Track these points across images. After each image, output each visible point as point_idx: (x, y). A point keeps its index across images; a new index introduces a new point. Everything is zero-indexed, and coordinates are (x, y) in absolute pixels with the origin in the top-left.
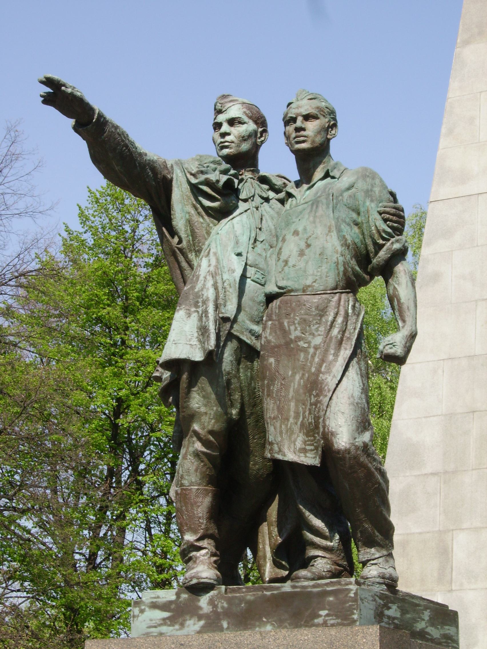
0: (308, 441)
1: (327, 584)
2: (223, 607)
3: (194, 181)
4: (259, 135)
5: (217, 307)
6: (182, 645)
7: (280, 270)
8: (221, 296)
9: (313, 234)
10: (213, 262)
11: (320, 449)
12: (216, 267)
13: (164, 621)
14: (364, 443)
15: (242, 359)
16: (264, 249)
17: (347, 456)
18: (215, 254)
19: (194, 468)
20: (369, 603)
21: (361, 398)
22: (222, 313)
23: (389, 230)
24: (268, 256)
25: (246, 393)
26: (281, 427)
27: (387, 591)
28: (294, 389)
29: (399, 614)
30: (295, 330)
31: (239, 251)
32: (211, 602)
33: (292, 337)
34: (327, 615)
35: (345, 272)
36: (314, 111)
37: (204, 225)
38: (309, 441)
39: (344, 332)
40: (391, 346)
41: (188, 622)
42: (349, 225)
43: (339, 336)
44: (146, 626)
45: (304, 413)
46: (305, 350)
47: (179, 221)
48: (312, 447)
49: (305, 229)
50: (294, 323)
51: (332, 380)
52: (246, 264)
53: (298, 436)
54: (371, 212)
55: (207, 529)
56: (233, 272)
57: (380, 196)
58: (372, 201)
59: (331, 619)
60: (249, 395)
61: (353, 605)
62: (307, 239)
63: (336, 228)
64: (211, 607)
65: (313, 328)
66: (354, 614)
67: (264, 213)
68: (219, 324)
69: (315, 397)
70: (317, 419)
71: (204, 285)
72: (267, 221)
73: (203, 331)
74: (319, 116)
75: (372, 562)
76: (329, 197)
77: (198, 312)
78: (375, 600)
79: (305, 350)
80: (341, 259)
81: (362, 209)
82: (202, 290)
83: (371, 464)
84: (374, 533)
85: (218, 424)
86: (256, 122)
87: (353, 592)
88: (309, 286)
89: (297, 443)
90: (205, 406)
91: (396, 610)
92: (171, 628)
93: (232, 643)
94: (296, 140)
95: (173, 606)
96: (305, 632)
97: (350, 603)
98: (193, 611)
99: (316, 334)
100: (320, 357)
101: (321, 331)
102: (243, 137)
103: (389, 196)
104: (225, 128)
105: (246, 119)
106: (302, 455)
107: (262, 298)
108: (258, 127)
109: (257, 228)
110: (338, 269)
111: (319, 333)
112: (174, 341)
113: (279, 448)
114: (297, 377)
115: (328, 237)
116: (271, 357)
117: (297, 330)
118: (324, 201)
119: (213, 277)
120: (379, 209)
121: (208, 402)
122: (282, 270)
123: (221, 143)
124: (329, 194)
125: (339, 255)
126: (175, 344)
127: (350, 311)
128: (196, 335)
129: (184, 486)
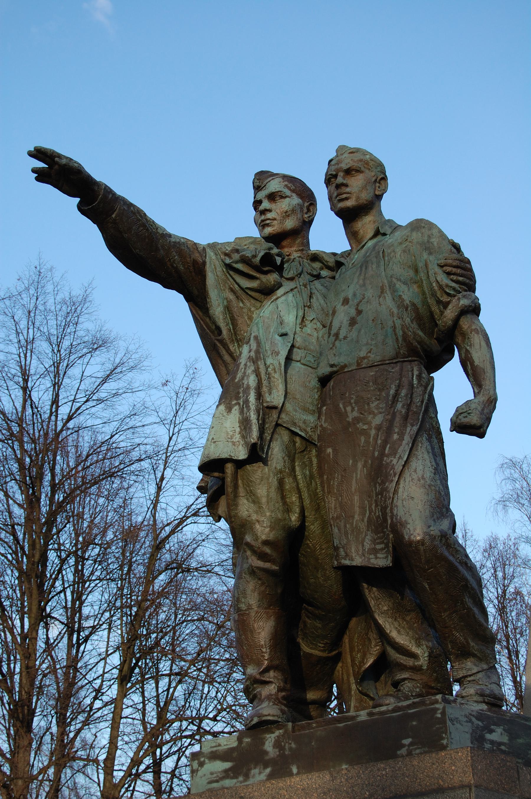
0: (377, 539)
1: (409, 707)
2: (291, 749)
3: (228, 261)
4: (305, 210)
5: (259, 396)
7: (331, 346)
8: (265, 383)
9: (363, 299)
10: (254, 346)
11: (390, 545)
12: (257, 352)
13: (227, 774)
14: (441, 531)
15: (297, 456)
16: (315, 329)
17: (422, 548)
18: (256, 338)
20: (462, 725)
21: (434, 479)
22: (267, 402)
23: (453, 284)
24: (320, 335)
26: (345, 526)
27: (489, 711)
28: (356, 480)
29: (507, 738)
31: (283, 331)
32: (277, 744)
33: (350, 419)
34: (411, 744)
35: (405, 337)
36: (356, 165)
39: (409, 405)
40: (466, 414)
41: (253, 772)
42: (405, 283)
43: (403, 411)
44: (207, 781)
45: (370, 507)
47: (217, 310)
48: (382, 546)
49: (355, 295)
50: (351, 404)
52: (293, 346)
53: (366, 535)
54: (430, 266)
55: (270, 659)
56: (278, 355)
58: (430, 253)
59: (416, 749)
60: (310, 496)
62: (358, 305)
63: (390, 288)
64: (277, 750)
65: (373, 405)
66: (443, 739)
68: (263, 414)
69: (380, 485)
70: (384, 509)
71: (245, 373)
72: (318, 299)
73: (245, 423)
74: (363, 169)
75: (469, 679)
76: (379, 254)
78: (470, 721)
79: (365, 433)
80: (398, 323)
81: (421, 265)
82: (243, 379)
83: (453, 556)
85: (273, 532)
87: (439, 711)
88: (364, 358)
89: (365, 544)
90: (256, 512)
91: (501, 734)
92: (235, 781)
93: (298, 789)
94: (338, 198)
95: (235, 754)
96: (382, 766)
97: (438, 726)
99: (376, 411)
100: (383, 438)
101: (382, 408)
102: (286, 212)
103: (450, 247)
104: (266, 204)
105: (288, 192)
106: (372, 556)
107: (314, 383)
108: (304, 202)
109: (305, 306)
110: (396, 334)
111: (380, 410)
112: (213, 439)
113: (346, 553)
114: (360, 465)
115: (381, 299)
116: (329, 447)
118: (374, 260)
119: (254, 362)
120: (439, 262)
123: (263, 221)
124: (379, 252)
127: (415, 382)
128: (238, 430)
129: (241, 610)
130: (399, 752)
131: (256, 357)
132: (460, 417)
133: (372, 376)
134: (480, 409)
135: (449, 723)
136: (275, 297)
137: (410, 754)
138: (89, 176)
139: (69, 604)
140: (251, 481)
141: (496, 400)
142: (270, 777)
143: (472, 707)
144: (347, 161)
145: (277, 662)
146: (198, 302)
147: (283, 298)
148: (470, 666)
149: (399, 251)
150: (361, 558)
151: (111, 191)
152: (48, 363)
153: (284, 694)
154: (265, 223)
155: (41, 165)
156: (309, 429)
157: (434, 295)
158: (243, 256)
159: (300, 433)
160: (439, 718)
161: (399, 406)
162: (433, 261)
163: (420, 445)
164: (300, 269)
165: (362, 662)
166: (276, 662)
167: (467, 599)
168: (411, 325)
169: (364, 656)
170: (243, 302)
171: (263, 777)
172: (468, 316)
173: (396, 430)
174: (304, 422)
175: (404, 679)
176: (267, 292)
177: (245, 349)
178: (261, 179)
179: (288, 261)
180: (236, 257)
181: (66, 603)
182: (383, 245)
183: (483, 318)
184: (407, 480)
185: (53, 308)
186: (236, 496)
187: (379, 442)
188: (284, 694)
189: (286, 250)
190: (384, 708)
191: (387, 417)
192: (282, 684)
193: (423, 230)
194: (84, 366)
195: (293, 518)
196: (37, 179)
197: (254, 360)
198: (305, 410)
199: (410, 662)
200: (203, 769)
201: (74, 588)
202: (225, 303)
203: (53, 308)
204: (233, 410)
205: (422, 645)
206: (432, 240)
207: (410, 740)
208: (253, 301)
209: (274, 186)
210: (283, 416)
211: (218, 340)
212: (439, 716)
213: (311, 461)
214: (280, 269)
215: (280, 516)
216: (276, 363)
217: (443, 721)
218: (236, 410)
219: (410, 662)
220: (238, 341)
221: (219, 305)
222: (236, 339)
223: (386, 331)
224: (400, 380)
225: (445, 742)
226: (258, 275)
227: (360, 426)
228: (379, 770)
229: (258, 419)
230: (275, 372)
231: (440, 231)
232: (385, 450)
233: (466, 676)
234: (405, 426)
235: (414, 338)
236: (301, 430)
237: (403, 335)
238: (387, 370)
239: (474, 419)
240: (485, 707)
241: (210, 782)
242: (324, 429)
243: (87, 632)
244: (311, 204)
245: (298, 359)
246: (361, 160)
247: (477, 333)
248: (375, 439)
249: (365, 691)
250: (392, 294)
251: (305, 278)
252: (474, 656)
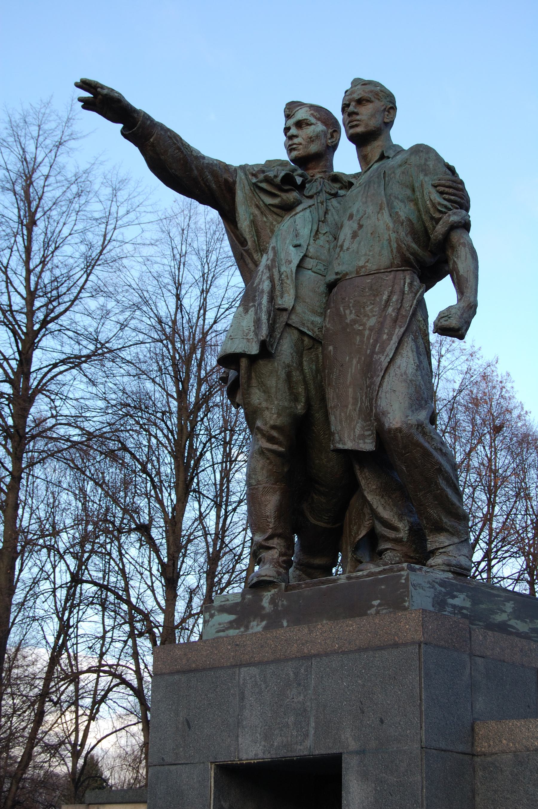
1: (380, 573)
4: (329, 136)
5: (272, 299)
6: (237, 645)
8: (278, 288)
9: (365, 214)
10: (271, 254)
12: (273, 260)
13: (232, 625)
15: (305, 352)
17: (399, 435)
18: (274, 248)
19: (260, 466)
20: (425, 590)
22: (280, 305)
23: (446, 203)
24: (332, 247)
25: (312, 387)
28: (351, 374)
31: (298, 243)
32: (272, 601)
34: (379, 605)
35: (399, 248)
37: (268, 224)
39: (399, 309)
40: (447, 318)
41: (252, 624)
42: (402, 201)
43: (394, 314)
46: (360, 333)
48: (370, 432)
49: (358, 211)
50: (349, 307)
52: (305, 256)
53: (357, 423)
54: (425, 186)
55: (275, 528)
57: (435, 170)
58: (426, 175)
59: (383, 609)
61: (405, 592)
62: (360, 220)
63: (388, 205)
65: (367, 309)
66: (405, 601)
67: (330, 208)
69: (370, 379)
71: (261, 279)
72: (332, 215)
73: (257, 322)
74: (373, 99)
78: (433, 587)
79: (360, 333)
80: (393, 236)
81: (417, 185)
82: (259, 284)
83: (429, 443)
84: (440, 519)
85: (280, 418)
86: (325, 123)
87: (404, 578)
88: (362, 267)
89: (356, 430)
90: (266, 401)
91: (464, 600)
92: (237, 631)
95: (238, 609)
96: (350, 622)
99: (370, 314)
101: (376, 312)
102: (311, 138)
103: (445, 169)
105: (313, 120)
106: (361, 441)
107: (323, 288)
109: (319, 221)
110: (391, 246)
111: (374, 313)
112: (231, 336)
114: (355, 362)
115: (380, 215)
118: (376, 180)
119: (269, 270)
120: (434, 182)
123: (290, 146)
125: (391, 232)
126: (232, 339)
127: (406, 289)
129: (251, 485)
130: (369, 612)
131: (272, 265)
132: (441, 321)
134: (459, 313)
135: (411, 587)
137: (378, 612)
138: (129, 105)
139: (218, 482)
140: (262, 374)
141: (476, 306)
142: (265, 628)
143: (438, 575)
144: (359, 92)
145: (281, 531)
146: (229, 217)
147: (301, 214)
148: (443, 539)
149: (398, 172)
150: (352, 442)
151: (149, 118)
152: (198, 275)
153: (285, 558)
155: (87, 95)
156: (316, 329)
157: (427, 211)
158: (266, 176)
159: (308, 332)
161: (390, 309)
162: (428, 181)
163: (406, 344)
164: (319, 188)
165: (357, 534)
166: (280, 531)
167: (441, 481)
168: (406, 238)
169: (359, 529)
170: (266, 217)
171: (259, 629)
172: (458, 231)
173: (386, 331)
174: (312, 323)
175: (387, 550)
176: (288, 208)
177: (265, 257)
178: (291, 108)
179: (310, 181)
180: (261, 176)
181: (215, 480)
182: (385, 167)
183: (472, 234)
184: (391, 375)
185: (203, 227)
186: (249, 386)
187: (371, 341)
188: (285, 558)
189: (311, 171)
190: (360, 573)
191: (379, 320)
192: (283, 550)
193: (421, 154)
194: (230, 277)
195: (299, 407)
196: (84, 107)
197: (269, 268)
198: (314, 312)
199: (392, 534)
201: (222, 467)
202: (252, 218)
203: (203, 227)
204: (250, 311)
205: (404, 520)
206: (428, 163)
207: (378, 601)
208: (275, 216)
209: (301, 114)
210: (293, 317)
211: (244, 250)
212: (403, 581)
213: (317, 357)
214: (301, 188)
215: (286, 404)
216: (288, 270)
217: (406, 586)
218: (252, 311)
219: (392, 534)
220: (261, 252)
221: (246, 220)
222: (260, 249)
224: (393, 286)
225: (406, 604)
226: (279, 193)
227: (356, 327)
228: (347, 626)
229: (268, 320)
230: (288, 279)
231: (437, 155)
232: (375, 348)
233: (439, 549)
234: (395, 328)
235: (408, 250)
236: (309, 330)
237: (397, 247)
238: (382, 278)
239: (453, 323)
240: (451, 575)
241: (218, 632)
242: (328, 330)
243: (234, 505)
244: (335, 131)
245: (310, 268)
246: (371, 92)
247: (465, 247)
248: (369, 339)
249: (359, 558)
250: (389, 211)
251: (323, 196)
252: (447, 531)
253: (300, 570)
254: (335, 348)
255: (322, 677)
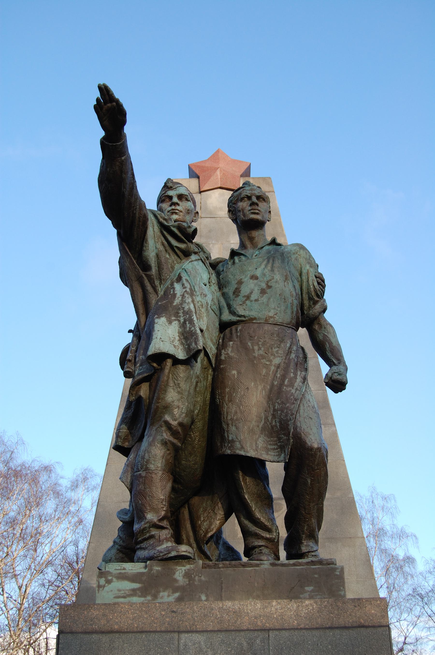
2: (200, 581)
6: (173, 612)
13: (134, 592)
19: (161, 454)
30: (258, 350)
32: (187, 575)
38: (272, 441)
41: (161, 594)
46: (267, 367)
50: (259, 345)
51: (295, 392)
66: (340, 590)
75: (313, 554)
77: (179, 321)
81: (304, 271)
82: (181, 304)
85: (187, 418)
88: (271, 317)
93: (229, 611)
94: (252, 211)
95: (144, 578)
98: (169, 584)
99: (276, 355)
102: (188, 210)
110: (292, 309)
112: (161, 338)
115: (286, 283)
117: (261, 350)
120: (316, 274)
121: (182, 398)
122: (244, 303)
125: (294, 299)
126: (162, 341)
128: (177, 338)
133: (276, 330)
136: (190, 260)
142: (179, 600)
154: (175, 211)
157: (309, 293)
160: (337, 575)
161: (293, 356)
200: (110, 586)
211: (146, 275)
223: (287, 305)
227: (263, 361)
230: (202, 307)
253: (123, 553)
254: (239, 373)
255: (282, 649)
